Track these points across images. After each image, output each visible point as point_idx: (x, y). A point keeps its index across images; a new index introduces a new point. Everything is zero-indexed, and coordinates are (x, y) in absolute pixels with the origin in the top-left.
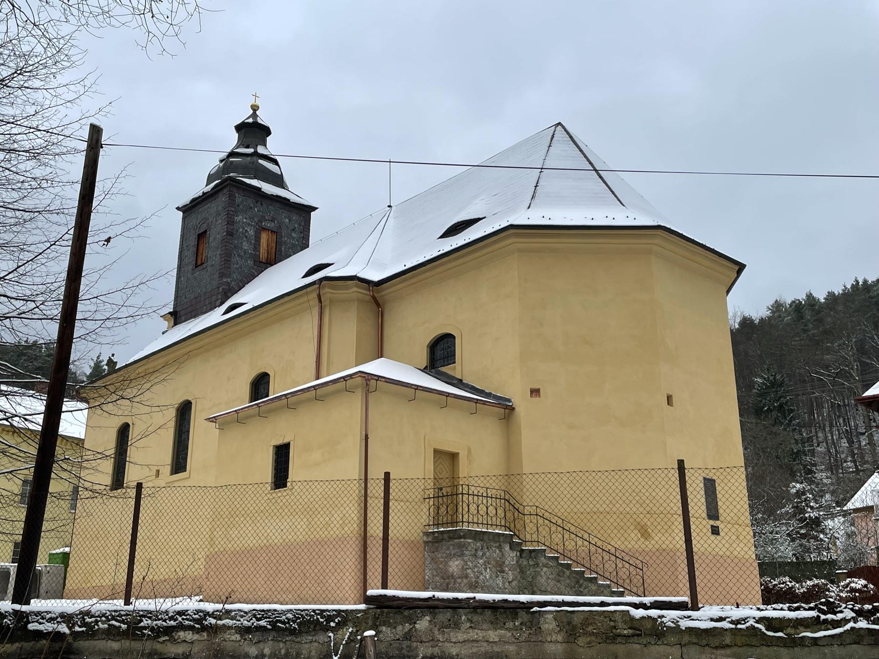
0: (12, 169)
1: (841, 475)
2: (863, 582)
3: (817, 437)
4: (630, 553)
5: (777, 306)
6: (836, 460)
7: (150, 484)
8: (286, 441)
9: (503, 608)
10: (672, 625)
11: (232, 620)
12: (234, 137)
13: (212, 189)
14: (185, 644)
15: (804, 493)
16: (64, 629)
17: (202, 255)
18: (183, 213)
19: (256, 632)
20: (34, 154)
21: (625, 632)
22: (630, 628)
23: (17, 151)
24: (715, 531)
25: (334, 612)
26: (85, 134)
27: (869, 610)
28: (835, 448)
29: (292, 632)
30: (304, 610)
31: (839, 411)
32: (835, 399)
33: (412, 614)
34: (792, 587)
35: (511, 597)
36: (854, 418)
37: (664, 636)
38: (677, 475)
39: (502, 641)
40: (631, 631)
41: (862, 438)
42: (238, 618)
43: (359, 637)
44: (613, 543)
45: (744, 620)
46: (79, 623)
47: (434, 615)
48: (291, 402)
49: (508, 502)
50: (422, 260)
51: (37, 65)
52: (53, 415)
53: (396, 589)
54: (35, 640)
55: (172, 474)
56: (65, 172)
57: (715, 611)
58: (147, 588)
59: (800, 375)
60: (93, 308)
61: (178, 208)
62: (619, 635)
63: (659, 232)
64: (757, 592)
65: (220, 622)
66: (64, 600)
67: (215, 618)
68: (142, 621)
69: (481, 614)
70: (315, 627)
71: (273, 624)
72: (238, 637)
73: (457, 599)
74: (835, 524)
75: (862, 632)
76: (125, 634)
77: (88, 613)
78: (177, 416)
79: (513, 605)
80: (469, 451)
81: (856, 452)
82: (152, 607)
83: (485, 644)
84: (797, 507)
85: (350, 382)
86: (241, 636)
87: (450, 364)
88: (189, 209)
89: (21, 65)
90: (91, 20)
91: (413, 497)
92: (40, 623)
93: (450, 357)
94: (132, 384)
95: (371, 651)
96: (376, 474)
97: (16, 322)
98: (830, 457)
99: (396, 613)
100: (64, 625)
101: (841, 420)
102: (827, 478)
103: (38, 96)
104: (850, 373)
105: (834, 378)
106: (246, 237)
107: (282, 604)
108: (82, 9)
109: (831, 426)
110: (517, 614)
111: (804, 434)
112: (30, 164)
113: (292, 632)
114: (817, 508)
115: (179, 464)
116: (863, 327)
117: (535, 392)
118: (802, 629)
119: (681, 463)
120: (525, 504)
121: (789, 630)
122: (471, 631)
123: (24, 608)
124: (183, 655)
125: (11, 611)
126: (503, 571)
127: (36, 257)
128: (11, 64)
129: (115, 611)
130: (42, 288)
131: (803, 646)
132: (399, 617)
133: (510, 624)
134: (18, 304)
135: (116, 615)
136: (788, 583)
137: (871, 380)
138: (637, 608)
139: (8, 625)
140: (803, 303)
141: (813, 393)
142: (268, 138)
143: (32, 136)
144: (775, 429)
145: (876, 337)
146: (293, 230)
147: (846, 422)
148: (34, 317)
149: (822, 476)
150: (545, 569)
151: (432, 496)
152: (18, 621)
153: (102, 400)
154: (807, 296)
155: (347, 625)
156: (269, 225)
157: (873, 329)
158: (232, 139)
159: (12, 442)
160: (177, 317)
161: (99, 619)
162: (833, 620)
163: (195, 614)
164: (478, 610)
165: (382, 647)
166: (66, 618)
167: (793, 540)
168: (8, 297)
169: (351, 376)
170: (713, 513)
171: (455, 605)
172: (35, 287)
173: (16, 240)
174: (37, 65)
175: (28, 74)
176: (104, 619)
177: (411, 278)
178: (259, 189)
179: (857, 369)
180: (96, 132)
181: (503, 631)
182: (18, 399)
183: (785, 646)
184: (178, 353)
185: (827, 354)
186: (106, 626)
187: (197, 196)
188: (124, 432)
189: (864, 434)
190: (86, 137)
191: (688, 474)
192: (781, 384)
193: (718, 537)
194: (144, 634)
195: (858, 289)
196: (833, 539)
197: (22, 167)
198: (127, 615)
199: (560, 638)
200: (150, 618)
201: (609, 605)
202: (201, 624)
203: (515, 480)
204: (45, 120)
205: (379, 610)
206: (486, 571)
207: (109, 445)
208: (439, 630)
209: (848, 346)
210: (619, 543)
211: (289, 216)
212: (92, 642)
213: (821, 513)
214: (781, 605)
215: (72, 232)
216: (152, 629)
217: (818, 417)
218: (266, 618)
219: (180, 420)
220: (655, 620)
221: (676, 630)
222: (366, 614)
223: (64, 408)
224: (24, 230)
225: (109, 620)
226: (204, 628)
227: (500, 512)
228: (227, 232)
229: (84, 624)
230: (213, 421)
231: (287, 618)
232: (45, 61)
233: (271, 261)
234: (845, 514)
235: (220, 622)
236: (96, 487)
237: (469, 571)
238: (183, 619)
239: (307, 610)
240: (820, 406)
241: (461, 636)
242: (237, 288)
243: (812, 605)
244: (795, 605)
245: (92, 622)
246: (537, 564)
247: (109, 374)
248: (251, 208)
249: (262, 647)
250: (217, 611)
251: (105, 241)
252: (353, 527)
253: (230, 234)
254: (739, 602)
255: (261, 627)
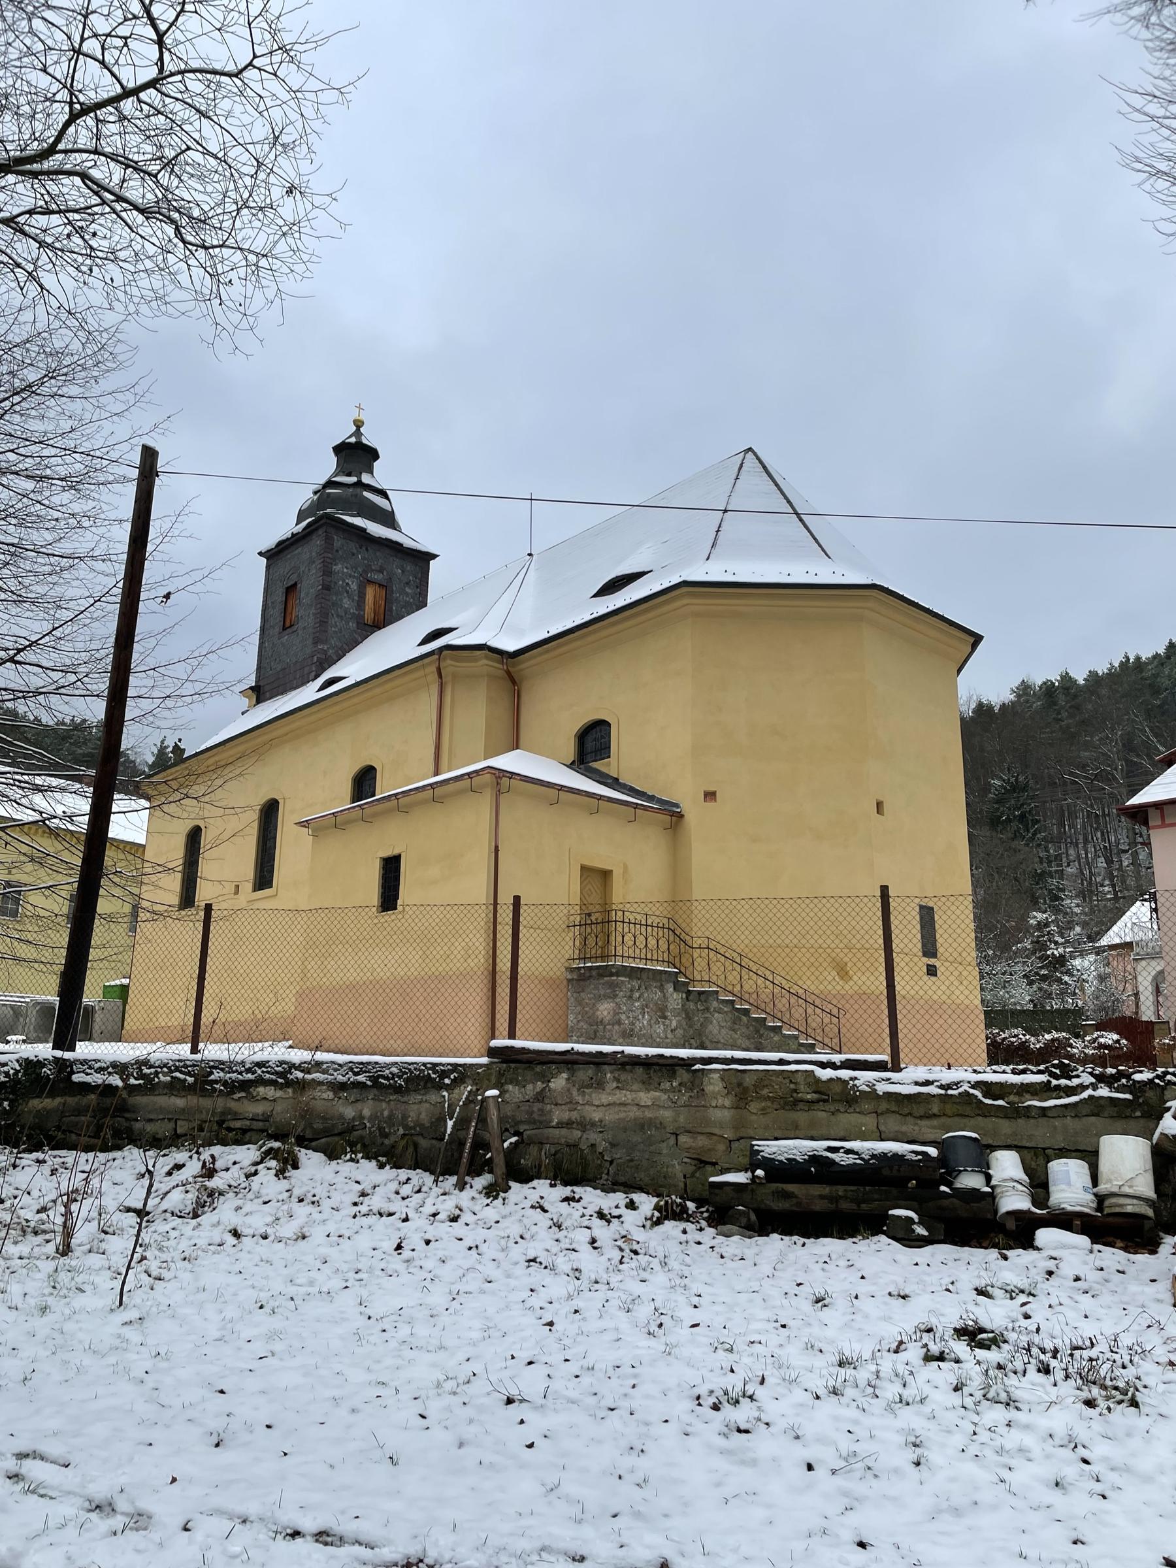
0: (43, 502)
1: (1096, 903)
2: (1116, 1037)
3: (1067, 855)
4: (821, 996)
5: (1024, 688)
6: (1090, 883)
7: (224, 905)
8: (396, 852)
9: (657, 1064)
10: (868, 1089)
11: (324, 1074)
12: (332, 461)
13: (305, 529)
14: (265, 1102)
15: (1047, 925)
16: (116, 1081)
17: (291, 614)
18: (268, 560)
19: (353, 1088)
20: (72, 484)
21: (809, 1097)
22: (815, 1092)
23: (49, 479)
24: (932, 971)
25: (449, 1067)
26: (136, 457)
27: (1112, 1075)
28: (1090, 868)
29: (398, 1090)
30: (413, 1063)
31: (1097, 822)
32: (1092, 807)
33: (544, 1070)
34: (1026, 1041)
35: (668, 1052)
36: (1115, 831)
37: (857, 1102)
38: (879, 905)
39: (656, 1105)
40: (815, 1096)
41: (1124, 856)
42: (331, 1071)
43: (479, 1098)
44: (800, 983)
45: (957, 1084)
46: (135, 1074)
47: (572, 1073)
48: (401, 803)
49: (673, 931)
50: (570, 625)
51: (73, 366)
52: (101, 814)
53: (526, 1039)
54: (81, 1094)
55: (255, 890)
56: (112, 507)
57: (921, 1073)
58: (218, 1031)
59: (1050, 776)
60: (150, 683)
61: (260, 554)
62: (802, 1101)
63: (875, 593)
64: (981, 1050)
65: (308, 1077)
66: (120, 1044)
67: (302, 1071)
68: (213, 1073)
69: (631, 1072)
70: (426, 1083)
71: (374, 1079)
72: (331, 1095)
73: (601, 1052)
74: (1084, 964)
75: (1102, 1102)
76: (191, 1089)
77: (146, 1063)
78: (260, 818)
79: (670, 1062)
80: (625, 867)
81: (1115, 874)
82: (224, 1056)
83: (635, 1108)
84: (1038, 942)
85: (476, 780)
86: (335, 1094)
87: (604, 759)
88: (275, 555)
89: (53, 366)
90: (144, 309)
91: (553, 922)
92: (87, 1074)
93: (603, 750)
94: (200, 780)
95: (493, 1115)
96: (505, 899)
97: (54, 699)
98: (1082, 880)
99: (525, 1069)
100: (117, 1077)
101: (1099, 834)
102: (1078, 906)
103: (76, 406)
104: (1113, 775)
105: (1092, 780)
106: (347, 592)
107: (384, 1055)
108: (129, 292)
109: (1086, 841)
110: (674, 1072)
111: (1051, 851)
112: (66, 497)
113: (398, 1090)
114: (1062, 944)
115: (264, 878)
116: (1133, 717)
117: (710, 795)
118: (1028, 1096)
119: (884, 890)
120: (693, 934)
121: (1012, 1098)
122: (618, 1092)
123: (68, 1055)
124: (263, 1115)
125: (51, 1058)
126: (665, 1017)
127: (76, 616)
128: (41, 365)
129: (179, 1061)
130: (85, 656)
131: (1028, 1117)
132: (529, 1075)
133: (667, 1085)
134: (56, 676)
135: (180, 1065)
136: (1021, 1036)
137: (1139, 785)
138: (824, 1068)
139: (48, 1075)
140: (1057, 684)
141: (1066, 800)
142: (375, 464)
143: (68, 459)
144: (1014, 844)
145: (1147, 730)
146: (407, 583)
147: (1105, 836)
148: (77, 692)
149: (1073, 904)
150: (716, 1015)
151: (577, 923)
152: (60, 1071)
153: (163, 799)
154: (1061, 676)
155: (464, 1082)
156: (377, 577)
157: (1145, 720)
158: (326, 466)
159: (51, 850)
160: (260, 693)
161: (159, 1070)
162: (1067, 1086)
163: (277, 1066)
164: (627, 1067)
165: (508, 1110)
166: (120, 1068)
167: (1031, 983)
168: (42, 667)
169: (477, 772)
170: (929, 948)
171: (598, 1060)
172: (76, 655)
173: (52, 593)
174: (73, 366)
175: (63, 378)
176: (165, 1070)
177: (555, 649)
178: (364, 530)
179: (1122, 770)
180: (149, 456)
181: (657, 1094)
182: (58, 796)
183: (1006, 1117)
184: (259, 740)
185: (1085, 750)
186: (168, 1078)
187: (284, 538)
188: (194, 837)
189: (1126, 851)
190: (138, 462)
191: (892, 904)
192: (1025, 788)
193: (933, 978)
194: (214, 1090)
195: (1128, 668)
196: (1081, 981)
197: (56, 500)
198: (194, 1066)
199: (727, 1103)
200: (222, 1070)
201: (789, 1063)
202: (285, 1078)
203: (684, 908)
204: (84, 439)
205: (505, 1065)
206: (643, 1017)
207: (176, 854)
208: (578, 1090)
209: (1112, 741)
210: (809, 983)
211: (402, 566)
212: (152, 1098)
213: (1068, 950)
214: (1004, 1067)
215: (121, 585)
216: (225, 1083)
217: (1070, 829)
218: (365, 1072)
219: (265, 823)
220: (845, 1082)
221: (872, 1095)
222: (488, 1069)
223: (115, 808)
224: (62, 581)
225: (172, 1072)
226: (289, 1084)
227: (664, 947)
228: (323, 585)
229: (142, 1076)
230: (305, 826)
231: (391, 1073)
232: (83, 361)
233: (378, 624)
234: (1098, 951)
235: (308, 1077)
236: (157, 908)
237: (623, 1017)
238: (263, 1072)
239: (415, 1063)
240: (1073, 816)
241: (605, 1098)
242: (335, 658)
243: (1042, 1067)
244: (1021, 1067)
245: (151, 1074)
246: (707, 1009)
247: (174, 765)
248: (353, 554)
249: (360, 1108)
250: (305, 1063)
251: (164, 597)
252: (479, 960)
253: (327, 588)
254: (951, 1061)
255: (360, 1083)
